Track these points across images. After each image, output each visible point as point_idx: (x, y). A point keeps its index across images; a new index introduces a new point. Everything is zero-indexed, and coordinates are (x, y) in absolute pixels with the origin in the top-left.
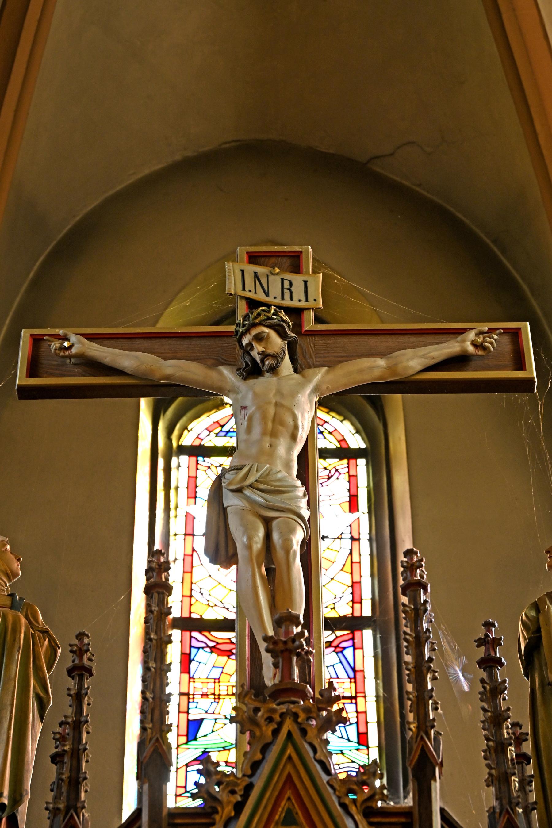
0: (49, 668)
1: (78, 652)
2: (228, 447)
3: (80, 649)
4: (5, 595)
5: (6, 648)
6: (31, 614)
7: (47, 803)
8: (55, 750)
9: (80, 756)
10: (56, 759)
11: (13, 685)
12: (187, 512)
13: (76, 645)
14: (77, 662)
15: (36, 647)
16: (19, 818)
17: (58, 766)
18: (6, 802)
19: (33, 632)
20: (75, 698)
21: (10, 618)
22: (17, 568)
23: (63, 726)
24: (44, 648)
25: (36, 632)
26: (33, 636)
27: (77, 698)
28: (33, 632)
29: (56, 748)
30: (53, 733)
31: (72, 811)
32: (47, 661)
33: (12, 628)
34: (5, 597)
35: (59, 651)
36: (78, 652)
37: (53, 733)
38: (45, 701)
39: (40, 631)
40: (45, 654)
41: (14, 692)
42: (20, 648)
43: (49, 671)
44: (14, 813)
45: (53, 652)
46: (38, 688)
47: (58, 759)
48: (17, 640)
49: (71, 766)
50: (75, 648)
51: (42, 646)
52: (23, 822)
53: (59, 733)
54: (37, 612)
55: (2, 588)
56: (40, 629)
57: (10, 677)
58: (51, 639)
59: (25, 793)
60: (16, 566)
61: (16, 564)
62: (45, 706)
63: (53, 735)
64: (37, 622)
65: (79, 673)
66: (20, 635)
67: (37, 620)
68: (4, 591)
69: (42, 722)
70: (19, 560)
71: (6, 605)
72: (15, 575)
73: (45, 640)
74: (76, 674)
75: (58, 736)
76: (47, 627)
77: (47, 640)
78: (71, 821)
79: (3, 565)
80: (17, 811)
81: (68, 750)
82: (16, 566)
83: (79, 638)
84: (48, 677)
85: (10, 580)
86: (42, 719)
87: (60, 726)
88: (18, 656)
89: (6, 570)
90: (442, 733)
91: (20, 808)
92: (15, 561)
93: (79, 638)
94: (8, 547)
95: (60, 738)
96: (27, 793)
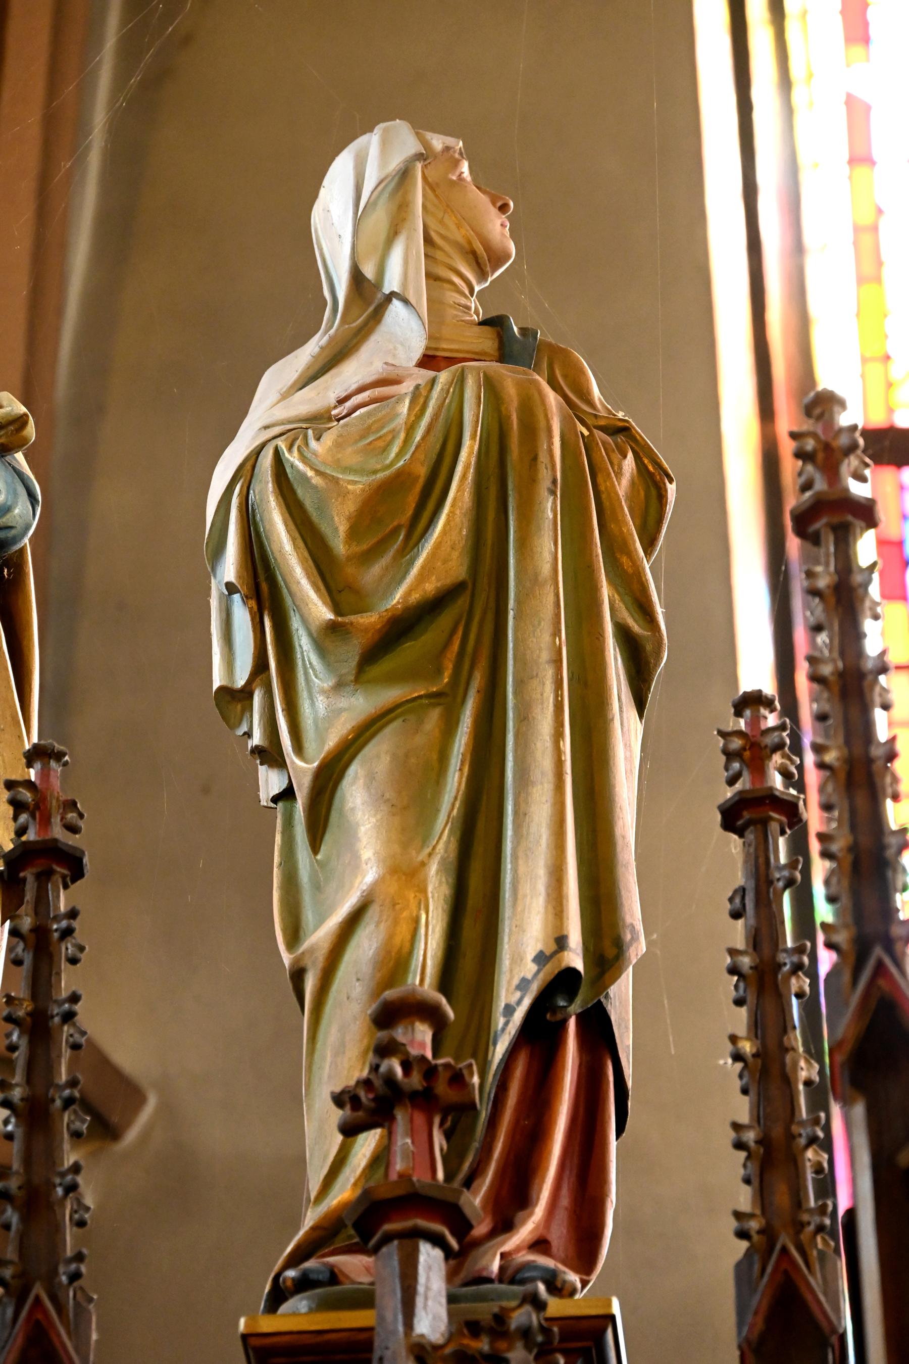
0: (649, 544)
1: (820, 456)
2: (362, 134)
3: (827, 447)
4: (472, 323)
5: (510, 486)
6: (565, 377)
7: (732, 952)
8: (729, 793)
9: (877, 780)
10: (740, 816)
11: (551, 598)
12: (849, 96)
13: (814, 435)
14: (820, 485)
15: (600, 479)
16: (613, 1018)
17: (750, 836)
18: (578, 964)
19: (586, 433)
20: (832, 600)
21: (511, 391)
22: (503, 235)
23: (748, 713)
24: (625, 481)
25: (596, 432)
26: (589, 444)
27: (839, 601)
28: (586, 433)
29: (731, 782)
30: (722, 734)
31: (878, 951)
32: (638, 522)
33: (520, 420)
34: (477, 329)
35: (671, 489)
36: (820, 456)
37: (722, 734)
38: (649, 648)
39: (602, 429)
40: (630, 498)
41: (559, 622)
42: (554, 482)
43: (648, 553)
44: (600, 1002)
45: (654, 492)
46: (619, 604)
47: (746, 815)
48: (543, 458)
49: (853, 812)
50: (810, 445)
51: (619, 474)
52: (627, 1028)
53: (739, 733)
54: (582, 372)
55: (463, 301)
56: (602, 423)
57: (536, 575)
58: (642, 453)
59: (628, 937)
60: (498, 228)
61: (498, 223)
62: (648, 663)
63: (721, 742)
64: (590, 403)
65: (836, 520)
66: (550, 444)
67: (586, 397)
68: (469, 308)
69: (641, 716)
70: (503, 208)
71: (485, 353)
72: (498, 258)
73: (625, 457)
74: (828, 525)
75: (736, 744)
76: (620, 415)
77: (630, 455)
78: (881, 982)
79: (459, 226)
80: (607, 996)
81: (836, 764)
82: (498, 228)
83: (817, 411)
84: (647, 567)
85: (482, 275)
86: (640, 705)
87: (738, 713)
88: (549, 508)
89: (470, 243)
90: (95, 1297)
91: (612, 987)
92: (493, 211)
93: (817, 411)
94: (465, 167)
95: (744, 749)
96: (635, 938)
